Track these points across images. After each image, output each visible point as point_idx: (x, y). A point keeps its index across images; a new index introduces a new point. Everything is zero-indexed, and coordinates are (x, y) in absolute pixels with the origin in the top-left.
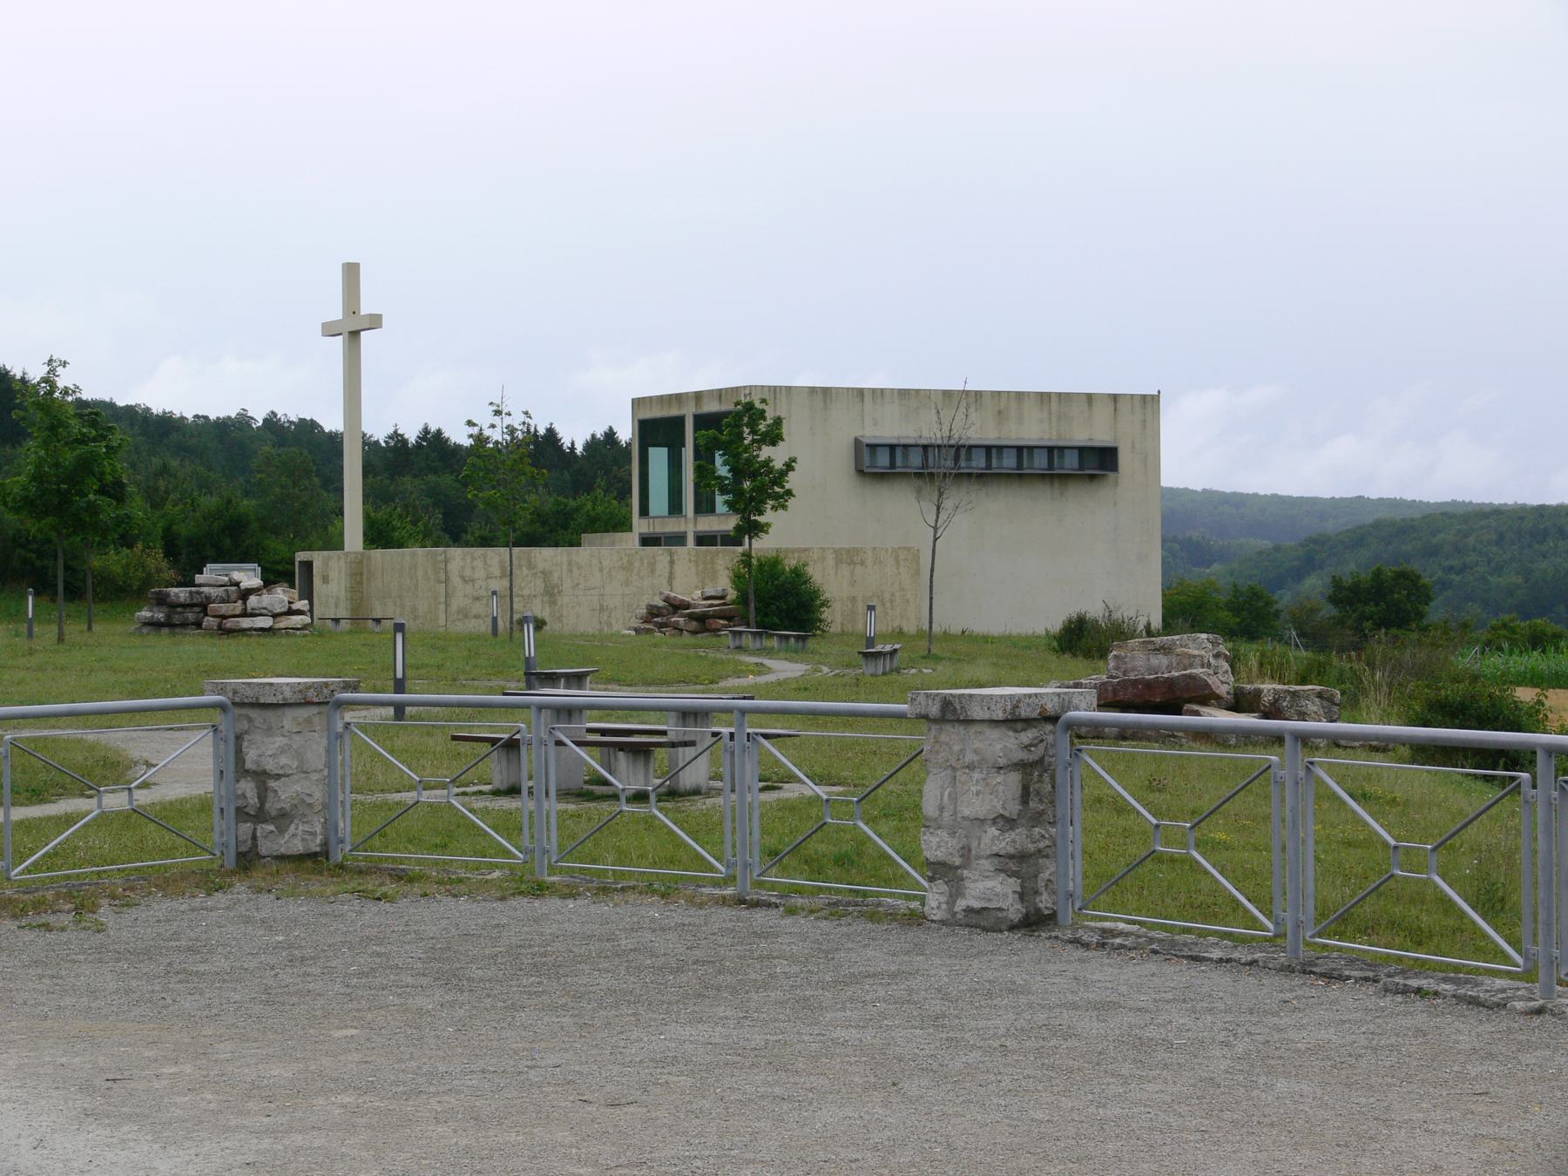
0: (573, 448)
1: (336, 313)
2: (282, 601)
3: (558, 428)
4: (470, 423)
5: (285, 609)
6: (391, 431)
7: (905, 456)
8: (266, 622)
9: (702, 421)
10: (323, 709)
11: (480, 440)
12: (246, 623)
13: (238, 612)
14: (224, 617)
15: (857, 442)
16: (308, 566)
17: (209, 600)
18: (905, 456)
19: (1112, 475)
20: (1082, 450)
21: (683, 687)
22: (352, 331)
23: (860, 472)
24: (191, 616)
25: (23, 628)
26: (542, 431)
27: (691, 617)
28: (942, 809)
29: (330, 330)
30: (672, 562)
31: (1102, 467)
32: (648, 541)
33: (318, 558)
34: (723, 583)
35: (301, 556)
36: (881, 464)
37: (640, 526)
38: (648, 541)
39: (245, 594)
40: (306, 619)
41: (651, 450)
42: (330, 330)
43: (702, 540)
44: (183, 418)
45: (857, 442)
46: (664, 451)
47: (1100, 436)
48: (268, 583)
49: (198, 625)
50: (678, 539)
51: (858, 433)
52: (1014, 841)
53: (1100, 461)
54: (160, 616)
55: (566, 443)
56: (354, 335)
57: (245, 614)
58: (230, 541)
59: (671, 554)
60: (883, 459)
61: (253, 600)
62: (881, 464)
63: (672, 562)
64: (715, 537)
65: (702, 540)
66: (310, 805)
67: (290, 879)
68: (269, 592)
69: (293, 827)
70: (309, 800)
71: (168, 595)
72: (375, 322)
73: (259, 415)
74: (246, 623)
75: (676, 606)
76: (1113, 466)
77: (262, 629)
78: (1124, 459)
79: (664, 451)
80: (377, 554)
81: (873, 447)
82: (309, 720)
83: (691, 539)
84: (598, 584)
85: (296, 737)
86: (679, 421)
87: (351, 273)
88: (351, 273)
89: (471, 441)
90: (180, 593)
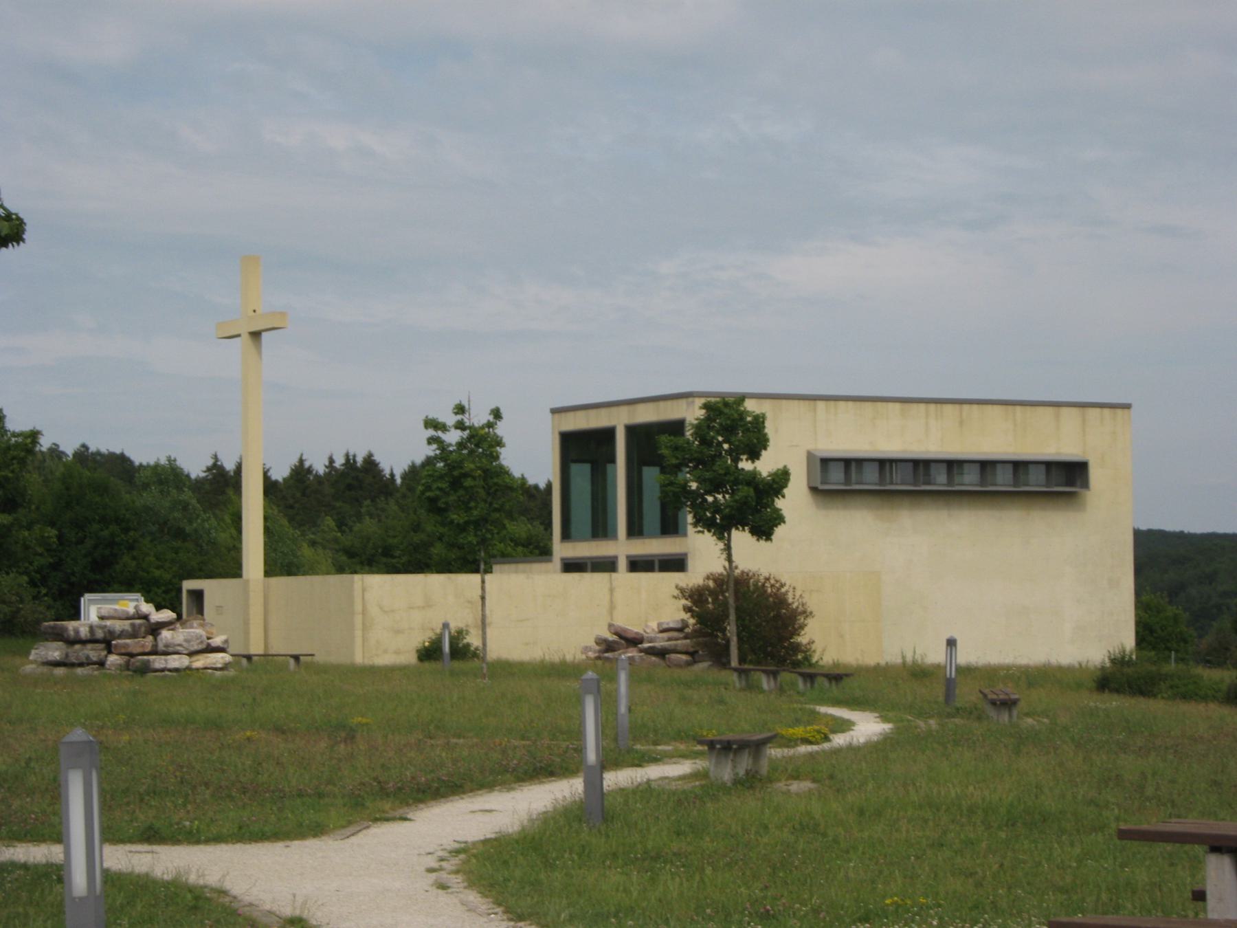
0: (392, 475)
2: (199, 637)
4: (497, 414)
5: (204, 646)
6: (210, 462)
8: (175, 662)
9: (642, 436)
13: (148, 649)
14: (132, 655)
16: (198, 596)
20: (1050, 466)
23: (814, 490)
24: (94, 656)
26: (360, 460)
30: (612, 590)
31: (1070, 483)
33: (209, 587)
34: (674, 613)
35: (188, 585)
36: (851, 481)
37: (562, 550)
38: (571, 566)
39: (155, 629)
41: (575, 468)
43: (638, 565)
46: (587, 468)
47: (1064, 448)
49: (101, 664)
51: (811, 447)
55: (387, 472)
57: (154, 652)
61: (166, 634)
62: (851, 481)
63: (612, 590)
64: (586, 564)
67: (165, 877)
71: (65, 629)
74: (158, 662)
75: (633, 641)
76: (1086, 485)
77: (177, 670)
78: (1095, 474)
79: (587, 468)
81: (825, 462)
83: (622, 564)
84: (538, 612)
86: (607, 435)
89: (703, 412)
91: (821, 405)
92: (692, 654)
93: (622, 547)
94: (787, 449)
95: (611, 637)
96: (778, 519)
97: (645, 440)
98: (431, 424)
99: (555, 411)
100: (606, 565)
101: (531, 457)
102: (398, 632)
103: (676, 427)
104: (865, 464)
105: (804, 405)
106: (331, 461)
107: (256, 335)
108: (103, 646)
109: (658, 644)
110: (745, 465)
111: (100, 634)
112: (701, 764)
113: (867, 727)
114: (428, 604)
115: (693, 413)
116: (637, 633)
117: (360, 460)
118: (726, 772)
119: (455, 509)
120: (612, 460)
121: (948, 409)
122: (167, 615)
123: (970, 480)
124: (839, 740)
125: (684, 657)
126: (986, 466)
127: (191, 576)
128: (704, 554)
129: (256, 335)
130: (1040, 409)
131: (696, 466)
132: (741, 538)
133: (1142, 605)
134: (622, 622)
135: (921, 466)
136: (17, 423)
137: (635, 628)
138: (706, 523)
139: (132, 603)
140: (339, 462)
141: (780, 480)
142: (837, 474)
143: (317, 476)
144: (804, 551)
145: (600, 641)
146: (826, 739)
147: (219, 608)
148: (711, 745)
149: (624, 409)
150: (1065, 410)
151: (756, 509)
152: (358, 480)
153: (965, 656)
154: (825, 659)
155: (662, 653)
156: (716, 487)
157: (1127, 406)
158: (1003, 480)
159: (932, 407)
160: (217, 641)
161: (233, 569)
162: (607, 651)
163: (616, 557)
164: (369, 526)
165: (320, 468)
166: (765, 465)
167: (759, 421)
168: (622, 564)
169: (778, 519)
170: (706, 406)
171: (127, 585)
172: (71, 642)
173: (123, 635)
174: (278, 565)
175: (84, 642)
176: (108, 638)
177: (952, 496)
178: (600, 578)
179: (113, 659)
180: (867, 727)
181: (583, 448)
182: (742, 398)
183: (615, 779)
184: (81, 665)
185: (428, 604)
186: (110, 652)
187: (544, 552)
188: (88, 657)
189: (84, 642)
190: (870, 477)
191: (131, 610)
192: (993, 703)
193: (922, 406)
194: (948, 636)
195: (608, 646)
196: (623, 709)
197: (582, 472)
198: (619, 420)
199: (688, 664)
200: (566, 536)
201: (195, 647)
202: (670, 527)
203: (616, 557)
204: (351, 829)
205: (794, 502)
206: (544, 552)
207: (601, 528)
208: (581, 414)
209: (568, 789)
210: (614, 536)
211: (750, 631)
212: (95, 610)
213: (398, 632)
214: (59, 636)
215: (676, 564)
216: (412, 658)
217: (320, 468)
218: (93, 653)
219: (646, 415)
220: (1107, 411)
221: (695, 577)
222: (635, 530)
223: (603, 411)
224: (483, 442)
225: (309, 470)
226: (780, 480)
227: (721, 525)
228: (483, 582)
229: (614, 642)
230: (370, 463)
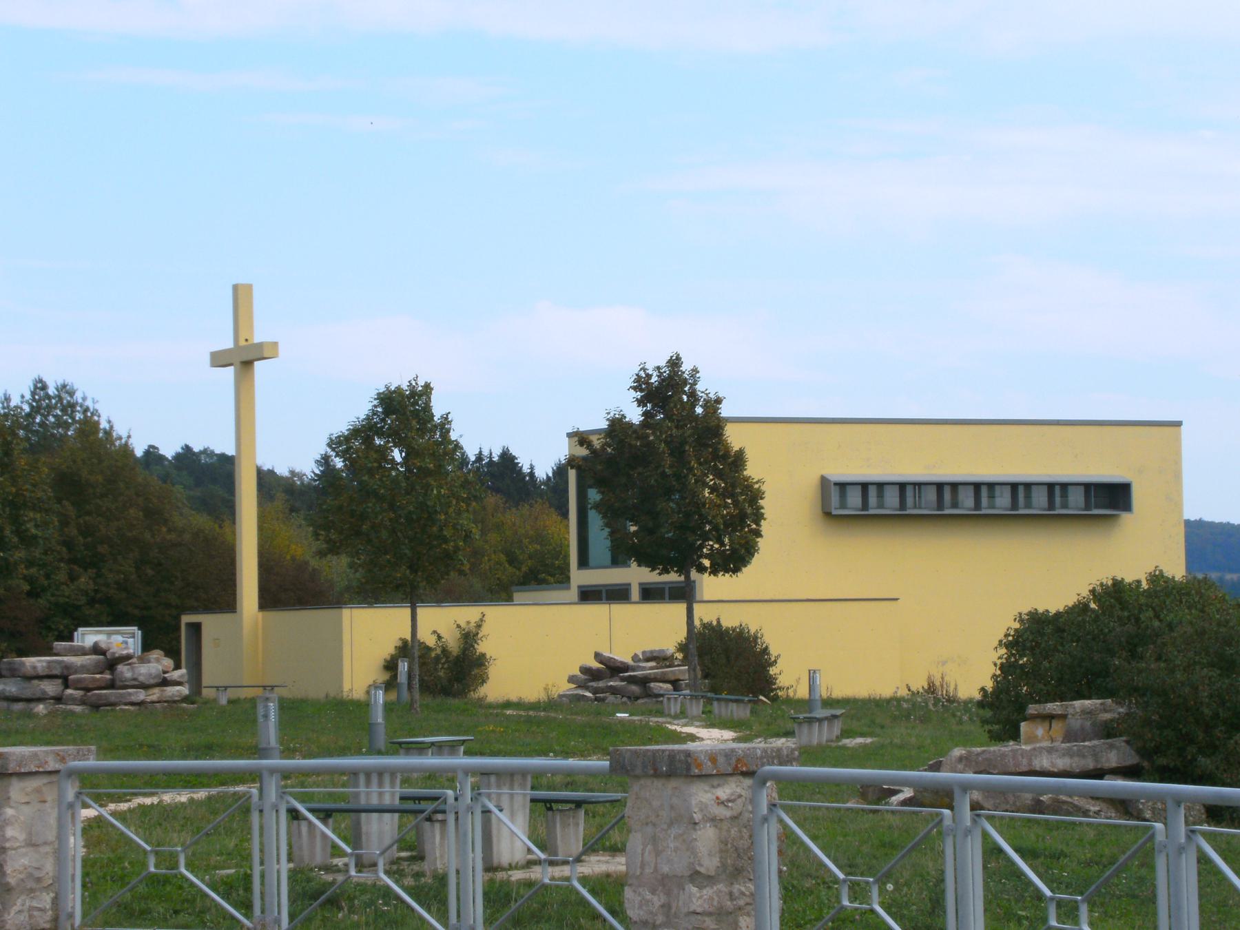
1: (226, 342)
3: (750, 455)
7: (991, 496)
10: (54, 778)
11: (532, 474)
14: (88, 690)
15: (824, 481)
16: (196, 628)
18: (880, 495)
19: (1125, 516)
21: (539, 755)
22: (243, 359)
23: (827, 514)
28: (643, 866)
29: (219, 360)
35: (186, 619)
36: (855, 506)
37: (580, 577)
38: (589, 595)
40: (184, 690)
42: (219, 360)
44: (617, 426)
48: (147, 646)
52: (711, 899)
55: (526, 470)
56: (247, 364)
57: (112, 685)
60: (854, 498)
62: (855, 506)
64: (600, 592)
66: (39, 880)
69: (19, 902)
70: (37, 874)
76: (1127, 507)
78: (1138, 496)
81: (843, 486)
82: (38, 791)
83: (635, 593)
85: (25, 809)
87: (241, 296)
88: (241, 296)
95: (596, 665)
100: (618, 594)
104: (848, 488)
108: (60, 681)
111: (57, 672)
116: (622, 663)
127: (194, 610)
136: (19, 393)
145: (585, 670)
154: (355, 687)
157: (1178, 424)
161: (226, 601)
162: (593, 680)
163: (629, 585)
168: (635, 593)
172: (29, 678)
173: (84, 669)
174: (270, 599)
176: (66, 673)
186: (67, 686)
187: (562, 578)
188: (44, 692)
196: (869, 740)
200: (583, 563)
203: (629, 585)
206: (562, 578)
212: (88, 637)
218: (51, 688)
229: (598, 670)
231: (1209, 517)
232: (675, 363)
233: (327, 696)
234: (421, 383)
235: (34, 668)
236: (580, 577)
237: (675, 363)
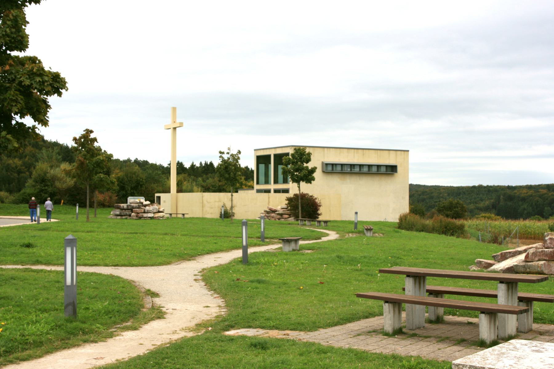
12: (145, 215)
14: (138, 213)
16: (159, 198)
17: (133, 208)
19: (396, 174)
20: (387, 166)
23: (323, 172)
24: (128, 213)
25: (75, 216)
26: (209, 163)
27: (278, 214)
30: (269, 198)
31: (392, 171)
32: (259, 191)
33: (162, 195)
35: (157, 195)
36: (331, 169)
38: (259, 191)
43: (276, 191)
45: (323, 163)
47: (392, 162)
49: (130, 215)
50: (268, 191)
51: (323, 160)
53: (392, 169)
54: (118, 213)
57: (145, 212)
58: (138, 189)
59: (232, 195)
62: (331, 169)
63: (269, 198)
65: (276, 191)
68: (152, 205)
72: (181, 125)
73: (133, 159)
74: (145, 215)
75: (274, 211)
76: (396, 171)
80: (181, 194)
81: (327, 164)
83: (272, 191)
84: (250, 204)
86: (269, 157)
90: (124, 206)
91: (326, 149)
92: (289, 215)
93: (272, 186)
94: (315, 162)
95: (268, 210)
96: (313, 179)
97: (279, 158)
98: (221, 153)
99: (255, 150)
100: (268, 191)
101: (248, 161)
102: (212, 208)
103: (287, 154)
105: (321, 149)
106: (201, 163)
107: (175, 128)
109: (280, 212)
110: (305, 165)
111: (130, 208)
112: (280, 245)
113: (333, 236)
114: (220, 201)
115: (291, 151)
117: (209, 163)
118: (288, 248)
119: (225, 176)
120: (270, 163)
121: (360, 151)
122: (148, 202)
123: (357, 169)
124: (324, 239)
125: (287, 216)
126: (370, 166)
128: (293, 188)
129: (175, 128)
130: (385, 151)
131: (294, 165)
132: (302, 184)
133: (411, 204)
134: (271, 207)
135: (352, 166)
137: (274, 208)
138: (294, 181)
139: (142, 200)
140: (203, 163)
141: (313, 170)
142: (330, 168)
143: (197, 167)
144: (319, 188)
145: (265, 211)
146: (320, 238)
147: (165, 202)
148: (283, 240)
149: (273, 150)
150: (391, 152)
151: (308, 177)
152: (208, 168)
153: (361, 218)
155: (281, 215)
156: (297, 170)
157: (408, 151)
158: (365, 169)
159: (356, 150)
160: (161, 210)
161: (168, 191)
164: (210, 181)
165: (198, 165)
166: (310, 165)
167: (309, 154)
168: (272, 191)
169: (313, 179)
170: (295, 149)
171: (140, 194)
175: (125, 209)
177: (360, 173)
178: (266, 195)
179: (133, 214)
180: (333, 236)
181: (262, 160)
182: (306, 147)
183: (251, 250)
184: (125, 216)
185: (220, 201)
187: (252, 188)
189: (125, 209)
190: (357, 169)
191: (138, 201)
192: (366, 229)
193: (353, 150)
194: (356, 211)
195: (267, 212)
197: (262, 166)
198: (272, 153)
199: (288, 218)
201: (155, 211)
202: (285, 181)
204: (179, 262)
205: (317, 175)
206: (252, 188)
207: (267, 182)
208: (262, 151)
209: (238, 254)
210: (270, 184)
211: (306, 209)
212: (131, 200)
213: (212, 208)
214: (118, 208)
215: (286, 191)
216: (217, 216)
217: (198, 165)
218: (128, 212)
219: (279, 151)
220: (402, 152)
221: (291, 194)
222: (276, 182)
223: (268, 150)
224: (235, 158)
225: (195, 165)
226: (313, 170)
227: (297, 180)
228: (232, 195)
230: (211, 164)
231: (415, 183)
232: (28, 23)
233: (316, 199)
234: (63, 91)
235: (123, 206)
236: (256, 187)
237: (28, 23)
